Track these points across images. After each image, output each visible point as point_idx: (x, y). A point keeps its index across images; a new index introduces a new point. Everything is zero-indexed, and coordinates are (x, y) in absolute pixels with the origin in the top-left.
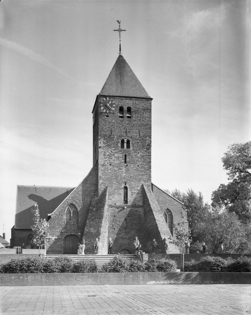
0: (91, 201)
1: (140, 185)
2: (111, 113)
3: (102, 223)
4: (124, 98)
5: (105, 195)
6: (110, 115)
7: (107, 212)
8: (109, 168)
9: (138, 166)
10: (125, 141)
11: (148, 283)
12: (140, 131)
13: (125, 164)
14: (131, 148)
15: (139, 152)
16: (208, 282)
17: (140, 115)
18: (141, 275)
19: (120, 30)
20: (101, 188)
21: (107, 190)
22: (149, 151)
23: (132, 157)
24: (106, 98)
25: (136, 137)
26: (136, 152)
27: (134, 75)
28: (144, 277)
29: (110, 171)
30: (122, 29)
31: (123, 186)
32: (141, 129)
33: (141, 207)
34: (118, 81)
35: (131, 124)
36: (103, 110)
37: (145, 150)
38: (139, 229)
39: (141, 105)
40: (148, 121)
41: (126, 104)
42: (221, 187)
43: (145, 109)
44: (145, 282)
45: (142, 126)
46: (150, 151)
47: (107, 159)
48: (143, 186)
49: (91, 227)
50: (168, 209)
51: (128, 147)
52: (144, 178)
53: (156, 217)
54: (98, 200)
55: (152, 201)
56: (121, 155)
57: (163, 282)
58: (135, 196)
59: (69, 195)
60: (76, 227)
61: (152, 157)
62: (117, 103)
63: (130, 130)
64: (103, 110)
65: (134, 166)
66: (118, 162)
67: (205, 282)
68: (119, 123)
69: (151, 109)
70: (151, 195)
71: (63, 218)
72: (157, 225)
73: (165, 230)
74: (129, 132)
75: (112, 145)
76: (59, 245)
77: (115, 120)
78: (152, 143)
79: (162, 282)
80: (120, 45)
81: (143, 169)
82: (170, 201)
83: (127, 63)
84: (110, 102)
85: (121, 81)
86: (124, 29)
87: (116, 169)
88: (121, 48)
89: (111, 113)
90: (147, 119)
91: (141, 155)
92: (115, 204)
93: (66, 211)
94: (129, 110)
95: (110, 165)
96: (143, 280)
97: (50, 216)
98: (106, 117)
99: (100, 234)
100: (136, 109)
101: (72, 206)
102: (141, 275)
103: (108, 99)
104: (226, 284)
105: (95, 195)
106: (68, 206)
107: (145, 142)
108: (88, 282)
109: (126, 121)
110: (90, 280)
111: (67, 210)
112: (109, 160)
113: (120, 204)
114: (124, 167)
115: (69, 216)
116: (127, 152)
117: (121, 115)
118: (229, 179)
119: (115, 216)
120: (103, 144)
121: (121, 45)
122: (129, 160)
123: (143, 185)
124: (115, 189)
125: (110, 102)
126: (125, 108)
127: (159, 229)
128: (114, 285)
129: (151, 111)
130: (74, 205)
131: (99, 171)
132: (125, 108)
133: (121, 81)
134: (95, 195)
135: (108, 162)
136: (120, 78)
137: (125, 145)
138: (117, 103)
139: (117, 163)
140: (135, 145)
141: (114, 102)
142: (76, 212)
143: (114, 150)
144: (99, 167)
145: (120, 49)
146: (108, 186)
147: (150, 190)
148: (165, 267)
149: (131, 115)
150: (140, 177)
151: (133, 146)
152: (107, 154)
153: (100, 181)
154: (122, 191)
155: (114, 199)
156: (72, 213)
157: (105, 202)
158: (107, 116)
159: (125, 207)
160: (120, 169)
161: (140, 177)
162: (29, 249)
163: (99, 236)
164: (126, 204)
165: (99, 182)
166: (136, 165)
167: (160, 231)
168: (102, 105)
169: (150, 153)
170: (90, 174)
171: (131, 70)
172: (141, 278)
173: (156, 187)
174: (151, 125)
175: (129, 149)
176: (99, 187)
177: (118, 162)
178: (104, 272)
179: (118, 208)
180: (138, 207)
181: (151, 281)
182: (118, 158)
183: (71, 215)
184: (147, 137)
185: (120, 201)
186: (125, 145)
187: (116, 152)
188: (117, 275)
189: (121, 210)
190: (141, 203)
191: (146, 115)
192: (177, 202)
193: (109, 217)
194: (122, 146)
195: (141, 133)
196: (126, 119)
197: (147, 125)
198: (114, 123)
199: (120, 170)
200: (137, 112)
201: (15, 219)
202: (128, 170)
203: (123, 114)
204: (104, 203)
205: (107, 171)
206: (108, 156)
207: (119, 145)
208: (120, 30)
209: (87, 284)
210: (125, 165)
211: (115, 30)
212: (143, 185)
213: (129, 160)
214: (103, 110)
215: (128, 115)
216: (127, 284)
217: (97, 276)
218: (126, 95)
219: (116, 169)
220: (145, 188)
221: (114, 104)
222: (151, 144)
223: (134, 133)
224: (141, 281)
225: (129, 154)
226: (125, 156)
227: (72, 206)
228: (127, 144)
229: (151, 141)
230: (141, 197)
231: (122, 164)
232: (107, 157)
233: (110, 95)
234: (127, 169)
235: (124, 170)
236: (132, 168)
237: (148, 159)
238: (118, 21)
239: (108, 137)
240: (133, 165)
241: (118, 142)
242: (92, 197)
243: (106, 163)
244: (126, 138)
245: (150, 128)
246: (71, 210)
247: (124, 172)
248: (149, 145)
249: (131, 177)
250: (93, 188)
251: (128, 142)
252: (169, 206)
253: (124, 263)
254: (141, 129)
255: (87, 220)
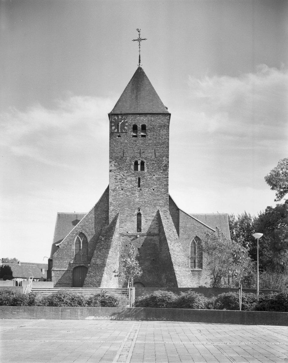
0: (101, 230)
1: (156, 211)
2: (124, 133)
3: (108, 253)
4: (138, 116)
5: (116, 223)
6: (122, 135)
7: (116, 240)
8: (120, 193)
9: (154, 190)
10: (139, 162)
11: (87, 318)
12: (156, 151)
13: (139, 188)
14: (146, 171)
15: (154, 174)
16: (152, 319)
17: (156, 132)
18: (79, 310)
19: (139, 40)
20: (112, 215)
21: (117, 217)
22: (166, 173)
23: (146, 180)
24: (118, 117)
25: (151, 157)
26: (151, 174)
27: (153, 88)
28: (82, 312)
29: (121, 196)
30: (142, 38)
31: (136, 212)
32: (157, 149)
33: (156, 235)
34: (134, 96)
35: (146, 143)
36: (115, 129)
37: (162, 171)
38: (153, 260)
39: (160, 120)
40: (165, 139)
41: (141, 121)
42: (268, 210)
43: (161, 126)
44: (83, 317)
45: (158, 145)
46: (168, 173)
47: (119, 183)
48: (159, 212)
49: (98, 258)
50: (197, 237)
51: (143, 169)
52: (160, 203)
53: (170, 246)
54: (108, 228)
55: (168, 228)
56: (134, 179)
57: (103, 318)
58: (150, 223)
59: (79, 223)
60: (86, 258)
61: (169, 179)
62: (131, 121)
63: (144, 151)
64: (126, 129)
65: (148, 191)
66: (131, 186)
67: (148, 319)
68: (132, 143)
69: (169, 126)
70: (168, 221)
71: (72, 248)
72: (170, 255)
73: (180, 260)
74: (144, 152)
75: (124, 168)
76: (67, 278)
77: (128, 141)
78: (169, 164)
79: (102, 317)
80: (140, 56)
81: (159, 193)
82: (199, 227)
83: (146, 75)
84: (123, 121)
85: (136, 96)
86: (144, 38)
87: (128, 193)
88: (141, 59)
89: (124, 133)
90: (164, 137)
91: (156, 178)
92: (127, 232)
93: (75, 241)
94: (144, 128)
95: (122, 189)
96: (82, 315)
97: (58, 246)
98: (118, 138)
99: (105, 266)
100: (151, 127)
101: (82, 236)
102: (79, 310)
103: (120, 117)
104: (168, 321)
105: (106, 223)
106: (77, 235)
107: (162, 163)
108: (24, 316)
109: (140, 140)
110: (26, 313)
111: (77, 240)
112: (121, 184)
113: (133, 233)
114: (138, 192)
115: (78, 245)
116: (141, 175)
117: (135, 134)
118: (275, 200)
119: (126, 246)
120: (114, 167)
121: (141, 56)
122: (143, 183)
123: (158, 211)
124: (127, 216)
125: (123, 121)
126: (139, 127)
127: (172, 259)
128: (50, 319)
129: (168, 128)
130: (83, 234)
131: (110, 197)
132: (139, 127)
133: (136, 96)
134: (106, 223)
135: (120, 186)
136: (137, 93)
137: (139, 167)
138: (131, 121)
139: (129, 187)
140: (151, 167)
141: (126, 120)
142: (85, 242)
143: (126, 173)
144: (110, 192)
145: (140, 60)
146: (120, 213)
147: (166, 217)
148: (108, 302)
149: (146, 133)
150: (155, 202)
151: (148, 168)
152: (118, 178)
153: (111, 208)
154: (135, 219)
155: (126, 227)
156: (81, 242)
157: (114, 230)
158: (119, 136)
159: (138, 236)
160: (133, 194)
161: (155, 202)
162: (42, 281)
163: (104, 267)
164: (139, 233)
165: (110, 208)
166: (151, 189)
167: (173, 262)
168: (113, 124)
169: (167, 174)
170: (101, 200)
171: (150, 83)
172: (79, 313)
173: (183, 212)
174: (169, 144)
175: (143, 171)
176: (110, 214)
177: (131, 186)
178: (43, 306)
179: (130, 236)
180: (153, 236)
181: (90, 316)
182: (131, 181)
183: (80, 245)
184: (163, 157)
185: (133, 229)
186: (139, 167)
187: (129, 176)
188: (54, 309)
189: (133, 239)
190: (156, 231)
191: (163, 132)
192: (207, 229)
193: (120, 246)
194: (136, 169)
195: (156, 154)
196: (140, 138)
197: (164, 143)
198: (126, 143)
199: (133, 195)
200: (153, 129)
201: (51, 249)
202: (142, 195)
203: (136, 132)
204: (113, 232)
205: (119, 196)
206: (119, 179)
207: (132, 167)
208: (139, 40)
209: (23, 318)
210: (139, 189)
211: (134, 40)
212: (158, 211)
213: (143, 183)
214: (115, 129)
215: (142, 134)
216: (64, 319)
217: (33, 310)
218: (141, 112)
219: (128, 193)
220: (161, 213)
221: (127, 122)
222: (168, 164)
223: (149, 154)
224: (79, 316)
225: (143, 177)
226: (139, 179)
227: (81, 235)
228: (141, 165)
229: (168, 161)
230: (157, 224)
231: (135, 188)
232: (118, 182)
233: (123, 112)
234: (141, 193)
235: (137, 194)
236: (147, 192)
237: (165, 182)
238: (138, 30)
239: (120, 159)
240: (147, 189)
241: (131, 164)
242: (104, 225)
243: (117, 188)
244: (139, 160)
245: (168, 147)
246: (81, 240)
247: (138, 196)
248: (167, 166)
249: (145, 202)
250: (104, 216)
251: (142, 163)
252: (198, 234)
253: (64, 298)
254: (157, 149)
255: (95, 250)
